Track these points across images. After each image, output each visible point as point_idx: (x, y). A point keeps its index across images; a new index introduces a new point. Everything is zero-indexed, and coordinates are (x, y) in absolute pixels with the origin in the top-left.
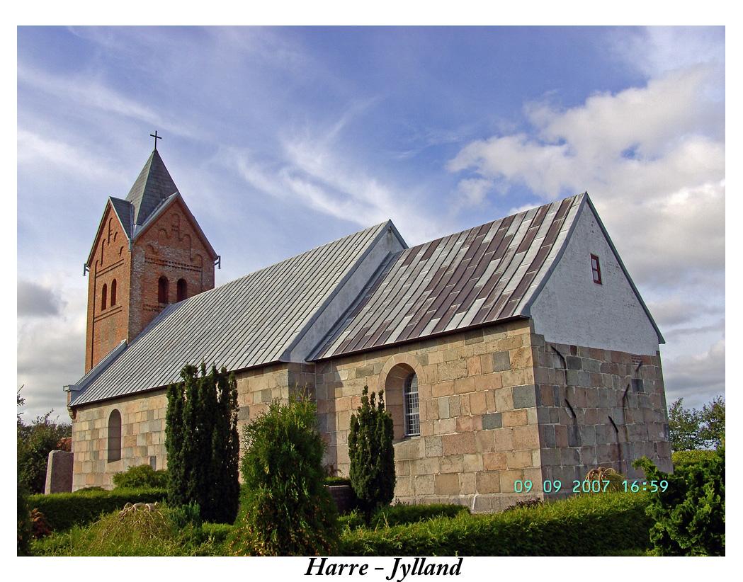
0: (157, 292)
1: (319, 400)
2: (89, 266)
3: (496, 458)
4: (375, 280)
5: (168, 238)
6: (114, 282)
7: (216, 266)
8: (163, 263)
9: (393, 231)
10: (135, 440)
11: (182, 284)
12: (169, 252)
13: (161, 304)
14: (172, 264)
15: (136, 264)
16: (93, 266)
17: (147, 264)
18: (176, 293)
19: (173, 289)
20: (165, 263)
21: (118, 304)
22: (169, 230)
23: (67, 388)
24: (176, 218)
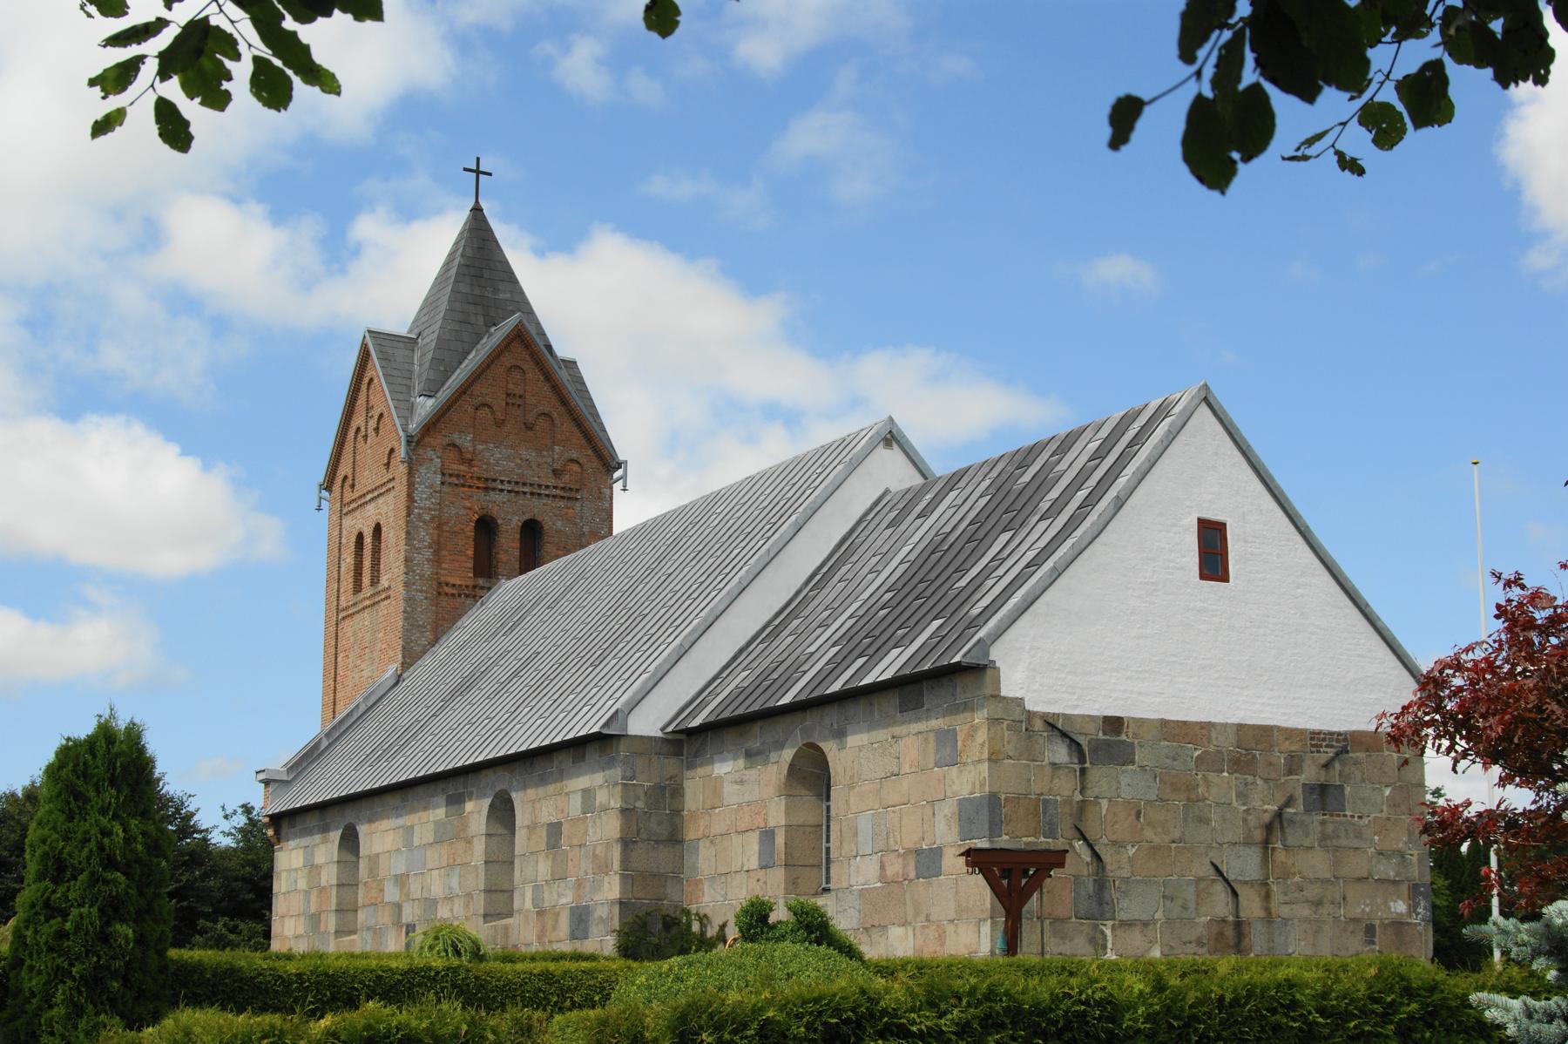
0: (470, 552)
1: (689, 811)
2: (329, 488)
3: (932, 933)
4: (843, 549)
5: (500, 424)
6: (378, 529)
7: (617, 487)
8: (488, 484)
9: (898, 442)
10: (382, 890)
11: (532, 531)
12: (500, 458)
13: (481, 582)
14: (507, 487)
15: (421, 493)
16: (337, 487)
17: (446, 489)
18: (517, 553)
19: (509, 544)
20: (490, 484)
21: (384, 582)
22: (499, 403)
23: (262, 776)
24: (517, 375)
